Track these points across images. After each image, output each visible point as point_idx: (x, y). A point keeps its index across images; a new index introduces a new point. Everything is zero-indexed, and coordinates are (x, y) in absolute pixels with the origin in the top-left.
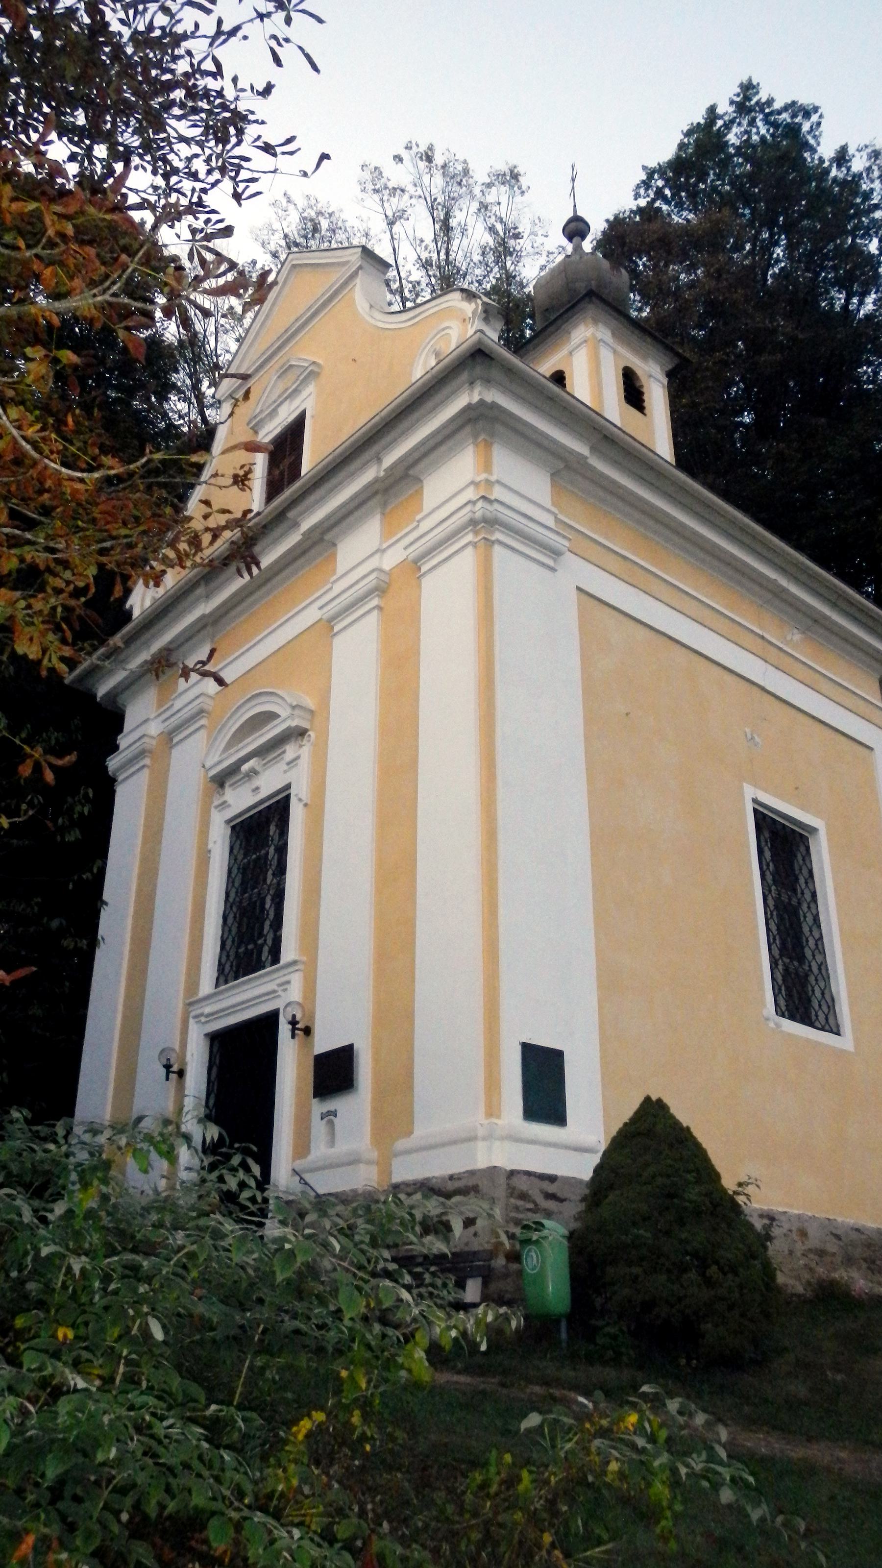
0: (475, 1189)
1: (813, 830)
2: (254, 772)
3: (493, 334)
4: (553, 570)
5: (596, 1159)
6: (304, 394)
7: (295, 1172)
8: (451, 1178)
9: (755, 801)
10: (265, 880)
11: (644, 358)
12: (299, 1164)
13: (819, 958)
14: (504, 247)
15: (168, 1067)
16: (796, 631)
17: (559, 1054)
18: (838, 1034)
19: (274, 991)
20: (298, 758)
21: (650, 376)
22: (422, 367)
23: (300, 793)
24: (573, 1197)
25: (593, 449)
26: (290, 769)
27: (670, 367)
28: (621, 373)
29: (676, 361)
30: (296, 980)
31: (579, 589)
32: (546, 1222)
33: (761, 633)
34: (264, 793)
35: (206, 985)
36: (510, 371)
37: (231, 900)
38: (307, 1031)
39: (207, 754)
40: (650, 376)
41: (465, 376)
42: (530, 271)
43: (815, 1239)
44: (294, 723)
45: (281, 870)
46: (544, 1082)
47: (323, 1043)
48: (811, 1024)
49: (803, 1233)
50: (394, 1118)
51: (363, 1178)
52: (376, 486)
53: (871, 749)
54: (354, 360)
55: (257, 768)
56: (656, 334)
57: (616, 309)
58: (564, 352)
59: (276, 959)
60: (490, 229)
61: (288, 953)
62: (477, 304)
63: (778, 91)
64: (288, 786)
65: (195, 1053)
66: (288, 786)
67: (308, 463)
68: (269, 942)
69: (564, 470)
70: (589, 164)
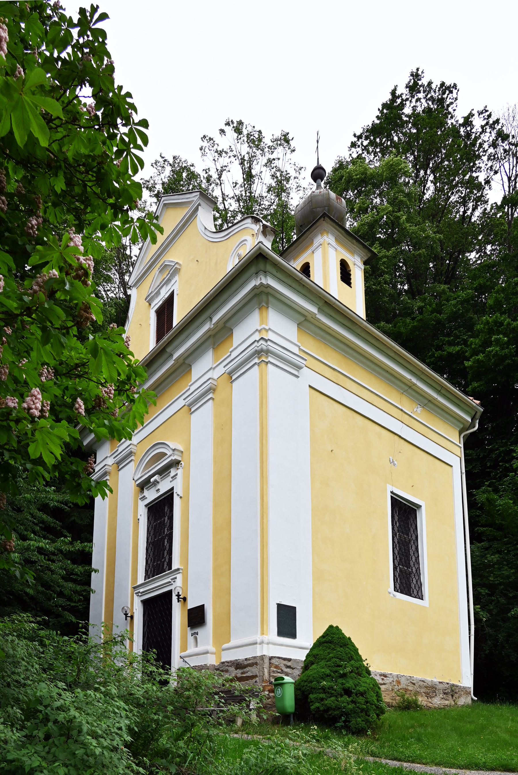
1: (419, 507)
2: (156, 482)
3: (268, 244)
4: (297, 377)
5: (307, 651)
6: (173, 282)
7: (181, 657)
8: (246, 659)
9: (392, 492)
10: (164, 532)
11: (352, 253)
12: (183, 654)
13: (417, 566)
14: (280, 188)
15: (126, 614)
16: (419, 406)
17: (294, 608)
18: (422, 599)
19: (170, 582)
20: (177, 475)
21: (355, 264)
22: (231, 264)
23: (178, 490)
24: (298, 667)
25: (320, 310)
27: (366, 258)
28: (339, 263)
29: (369, 255)
30: (179, 582)
31: (310, 386)
32: (285, 677)
33: (401, 407)
34: (162, 492)
35: (141, 580)
36: (276, 265)
37: (149, 541)
38: (185, 599)
39: (135, 474)
40: (355, 264)
41: (253, 270)
42: (295, 200)
43: (404, 683)
44: (173, 458)
45: (171, 527)
46: (287, 621)
47: (192, 604)
48: (410, 595)
49: (399, 682)
50: (223, 634)
52: (210, 333)
53: (452, 466)
54: (197, 261)
55: (158, 480)
56: (360, 239)
57: (339, 224)
58: (309, 251)
59: (170, 568)
60: (273, 176)
61: (174, 566)
62: (260, 225)
63: (433, 76)
64: (172, 489)
66: (172, 489)
67: (177, 319)
68: (167, 560)
69: (304, 322)
70: (326, 130)
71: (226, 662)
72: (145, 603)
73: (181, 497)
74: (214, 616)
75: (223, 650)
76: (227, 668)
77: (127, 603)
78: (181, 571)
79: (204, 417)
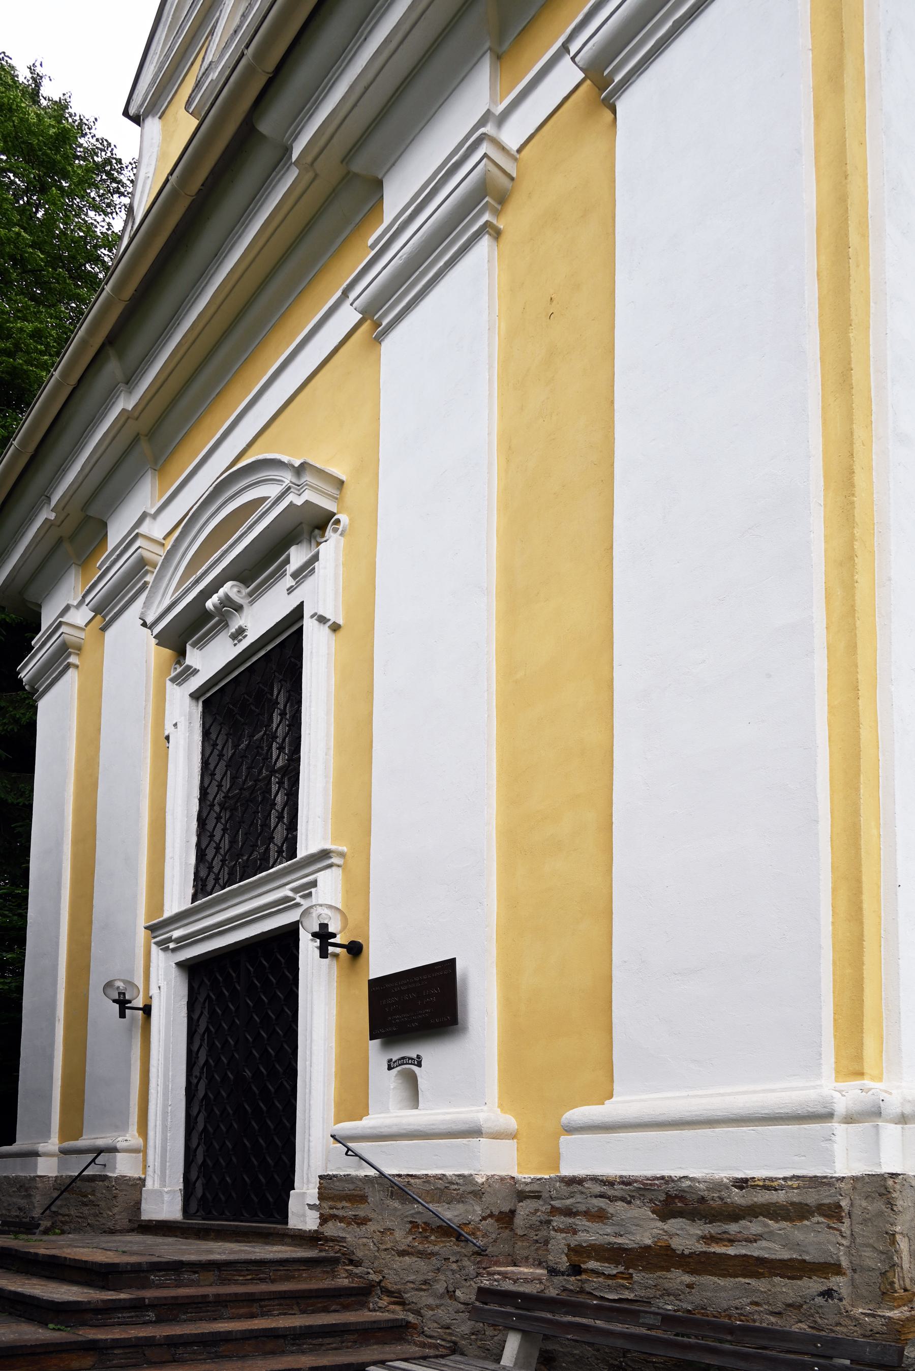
0: (833, 1212)
2: (231, 607)
8: (742, 1184)
12: (347, 1127)
15: (123, 1004)
19: (286, 899)
20: (315, 558)
26: (298, 584)
30: (329, 888)
34: (252, 636)
35: (178, 895)
38: (355, 949)
51: (496, 1161)
65: (163, 984)
71: (594, 1179)
72: (193, 970)
73: (335, 628)
74: (509, 1004)
75: (571, 1130)
76: (601, 1203)
77: (132, 971)
78: (335, 860)
79: (459, 323)
